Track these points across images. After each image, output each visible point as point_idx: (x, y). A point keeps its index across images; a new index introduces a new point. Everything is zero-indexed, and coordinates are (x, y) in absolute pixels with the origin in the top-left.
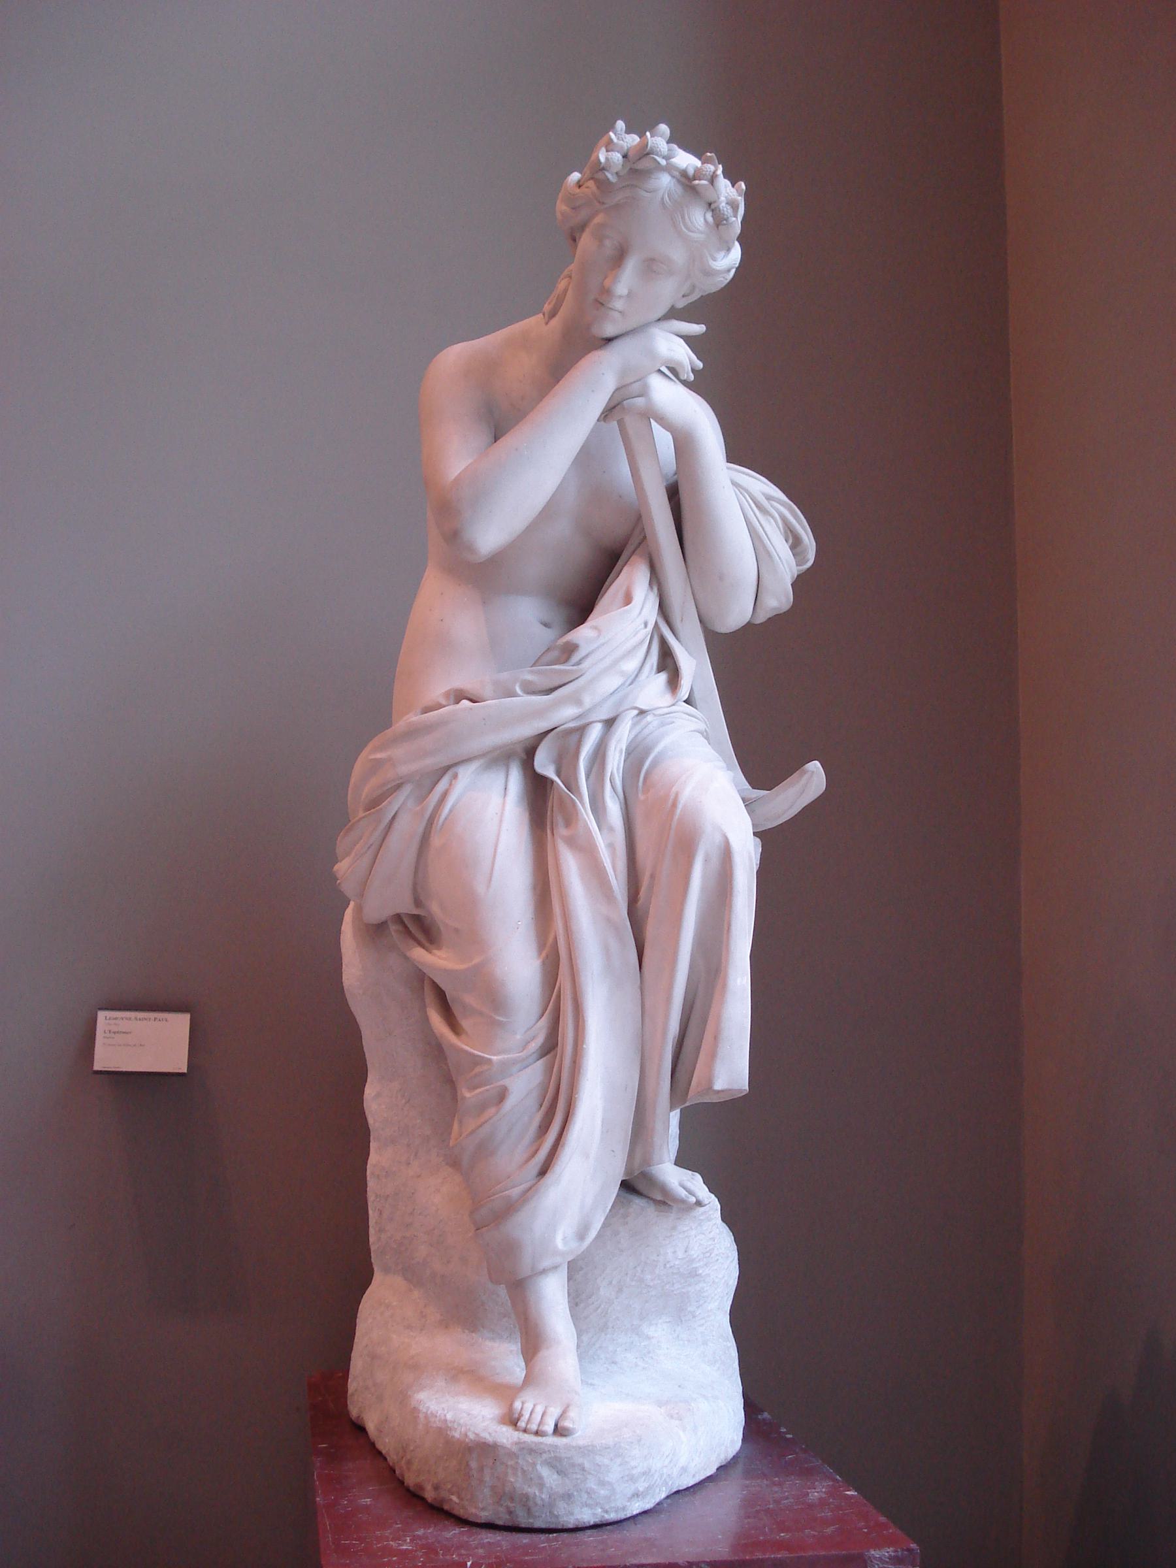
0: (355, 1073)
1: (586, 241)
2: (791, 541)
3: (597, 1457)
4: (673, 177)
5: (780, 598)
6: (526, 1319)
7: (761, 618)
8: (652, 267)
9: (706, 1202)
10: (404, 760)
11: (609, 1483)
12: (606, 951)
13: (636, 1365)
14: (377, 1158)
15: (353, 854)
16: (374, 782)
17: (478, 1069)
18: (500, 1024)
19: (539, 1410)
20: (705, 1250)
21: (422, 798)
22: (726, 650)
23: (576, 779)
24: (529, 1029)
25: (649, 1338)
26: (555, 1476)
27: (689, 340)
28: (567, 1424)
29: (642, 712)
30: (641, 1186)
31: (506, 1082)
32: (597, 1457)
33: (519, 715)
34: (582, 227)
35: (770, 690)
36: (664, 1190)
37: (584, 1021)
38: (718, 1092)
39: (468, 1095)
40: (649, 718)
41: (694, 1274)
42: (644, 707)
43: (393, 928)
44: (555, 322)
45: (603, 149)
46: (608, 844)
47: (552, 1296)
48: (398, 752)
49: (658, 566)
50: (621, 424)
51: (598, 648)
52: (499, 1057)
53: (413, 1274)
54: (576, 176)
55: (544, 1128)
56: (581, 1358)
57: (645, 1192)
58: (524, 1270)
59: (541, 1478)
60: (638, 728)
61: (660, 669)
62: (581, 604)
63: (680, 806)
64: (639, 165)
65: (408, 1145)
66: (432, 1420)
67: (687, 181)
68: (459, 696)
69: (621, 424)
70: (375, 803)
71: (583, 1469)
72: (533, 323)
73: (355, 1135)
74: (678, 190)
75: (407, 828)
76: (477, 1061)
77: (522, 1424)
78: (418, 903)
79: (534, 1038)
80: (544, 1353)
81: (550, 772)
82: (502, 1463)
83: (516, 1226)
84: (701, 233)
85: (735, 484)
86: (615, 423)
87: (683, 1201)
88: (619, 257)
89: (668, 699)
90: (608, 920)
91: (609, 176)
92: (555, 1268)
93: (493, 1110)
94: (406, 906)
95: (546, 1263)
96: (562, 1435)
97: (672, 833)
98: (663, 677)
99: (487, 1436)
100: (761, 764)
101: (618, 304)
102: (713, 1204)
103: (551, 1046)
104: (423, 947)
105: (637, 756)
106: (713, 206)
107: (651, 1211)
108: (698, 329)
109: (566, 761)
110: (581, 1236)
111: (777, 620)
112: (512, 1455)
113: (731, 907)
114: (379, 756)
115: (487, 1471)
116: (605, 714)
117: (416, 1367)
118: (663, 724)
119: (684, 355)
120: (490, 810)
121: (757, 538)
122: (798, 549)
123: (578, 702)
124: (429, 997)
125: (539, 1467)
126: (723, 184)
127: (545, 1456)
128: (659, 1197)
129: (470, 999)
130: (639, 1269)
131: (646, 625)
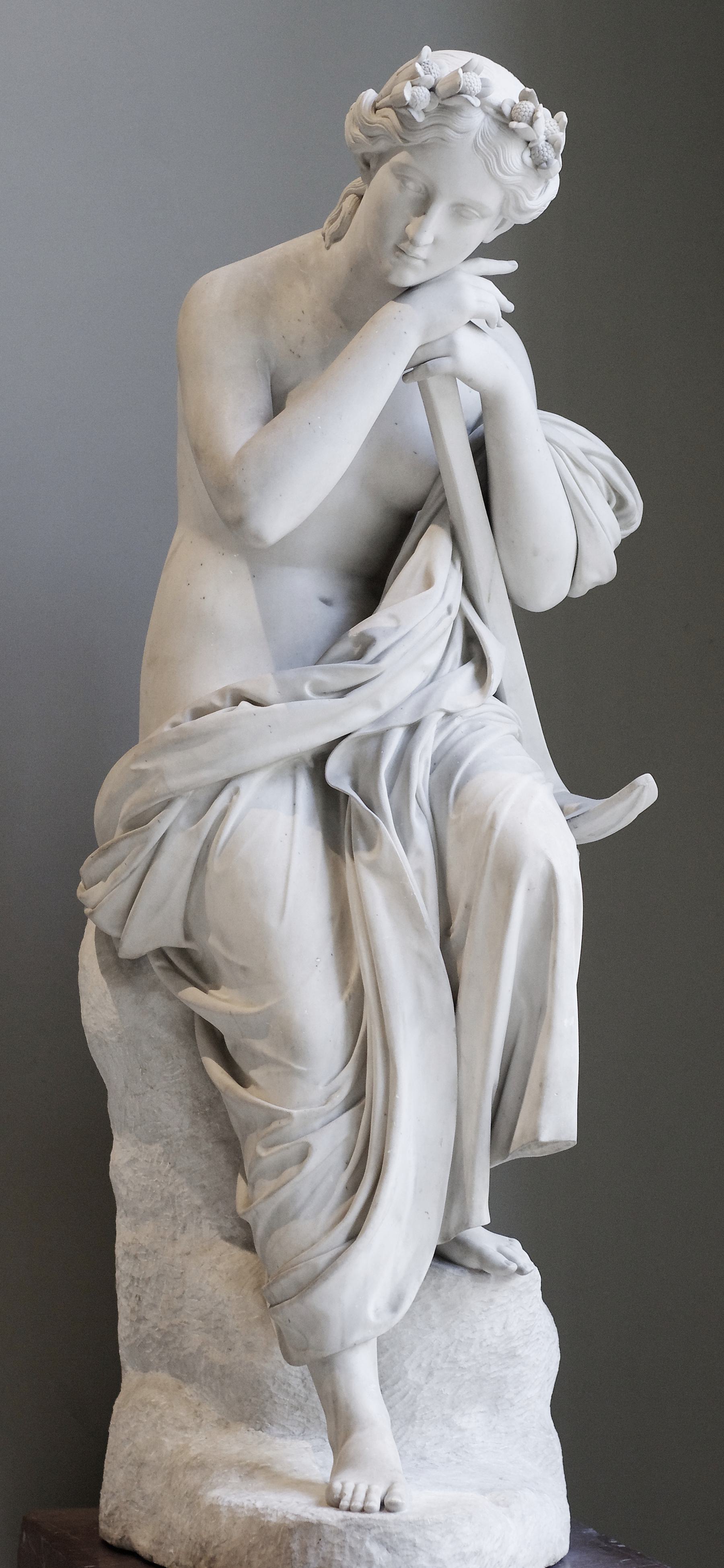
0: (94, 1137)
1: (383, 175)
2: (614, 502)
3: (428, 1533)
4: (487, 113)
5: (602, 569)
6: (335, 1401)
7: (581, 591)
8: (460, 212)
9: (528, 1269)
10: (178, 772)
11: (441, 1560)
12: (419, 991)
13: (449, 1460)
14: (126, 1233)
15: (110, 879)
16: (138, 795)
17: (275, 1125)
18: (299, 1074)
19: (362, 1489)
20: (517, 1328)
21: (198, 817)
22: (531, 627)
23: (377, 794)
24: (330, 1082)
25: (461, 1430)
26: (385, 1553)
27: (498, 280)
28: (395, 1499)
29: (448, 715)
30: (455, 1254)
31: (310, 1139)
32: (428, 1533)
33: (311, 723)
34: (382, 157)
35: (591, 678)
36: (482, 1257)
37: (395, 1068)
38: (546, 1144)
39: (262, 1153)
40: (457, 722)
41: (512, 1355)
42: (450, 709)
43: (156, 964)
44: (337, 247)
45: (409, 83)
46: (416, 867)
47: (361, 1374)
48: (169, 762)
49: (463, 543)
50: (424, 389)
51: (397, 642)
52: (302, 1111)
53: (183, 1369)
54: (370, 95)
55: (353, 1187)
56: (397, 1439)
57: (458, 1260)
58: (333, 1345)
59: (369, 1555)
60: (445, 734)
61: (466, 658)
62: (369, 581)
63: (498, 828)
64: (449, 98)
65: (174, 1218)
66: (240, 1511)
67: (504, 120)
68: (238, 698)
69: (424, 389)
70: (138, 822)
71: (415, 1545)
72: (309, 240)
73: (95, 1209)
74: (494, 128)
75: (179, 852)
76: (273, 1117)
77: (345, 1503)
78: (188, 936)
79: (337, 1090)
80: (356, 1436)
81: (344, 786)
82: (328, 1542)
83: (323, 1297)
84: (518, 175)
85: (548, 440)
86: (416, 383)
87: (503, 1268)
88: (424, 204)
89: (476, 695)
90: (420, 956)
91: (414, 114)
92: (365, 1341)
93: (293, 1170)
94: (173, 938)
95: (357, 1337)
96: (389, 1511)
97: (491, 859)
98: (469, 669)
99: (310, 1516)
100: (584, 768)
101: (422, 252)
102: (534, 1277)
103: (357, 1098)
104: (196, 985)
105: (446, 767)
106: (531, 145)
107: (467, 1279)
108: (509, 267)
109: (363, 772)
110: (394, 1308)
111: (597, 592)
112: (339, 1533)
113: (556, 941)
114: (143, 766)
115: (311, 1552)
116: (406, 717)
117: (200, 1465)
118: (472, 730)
119: (495, 301)
120: (277, 831)
121: (574, 505)
122: (621, 513)
123: (377, 705)
124: (202, 1042)
125: (367, 1544)
126: (543, 113)
127: (374, 1532)
128: (474, 1264)
129: (261, 1046)
130: (452, 1349)
131: (449, 610)
